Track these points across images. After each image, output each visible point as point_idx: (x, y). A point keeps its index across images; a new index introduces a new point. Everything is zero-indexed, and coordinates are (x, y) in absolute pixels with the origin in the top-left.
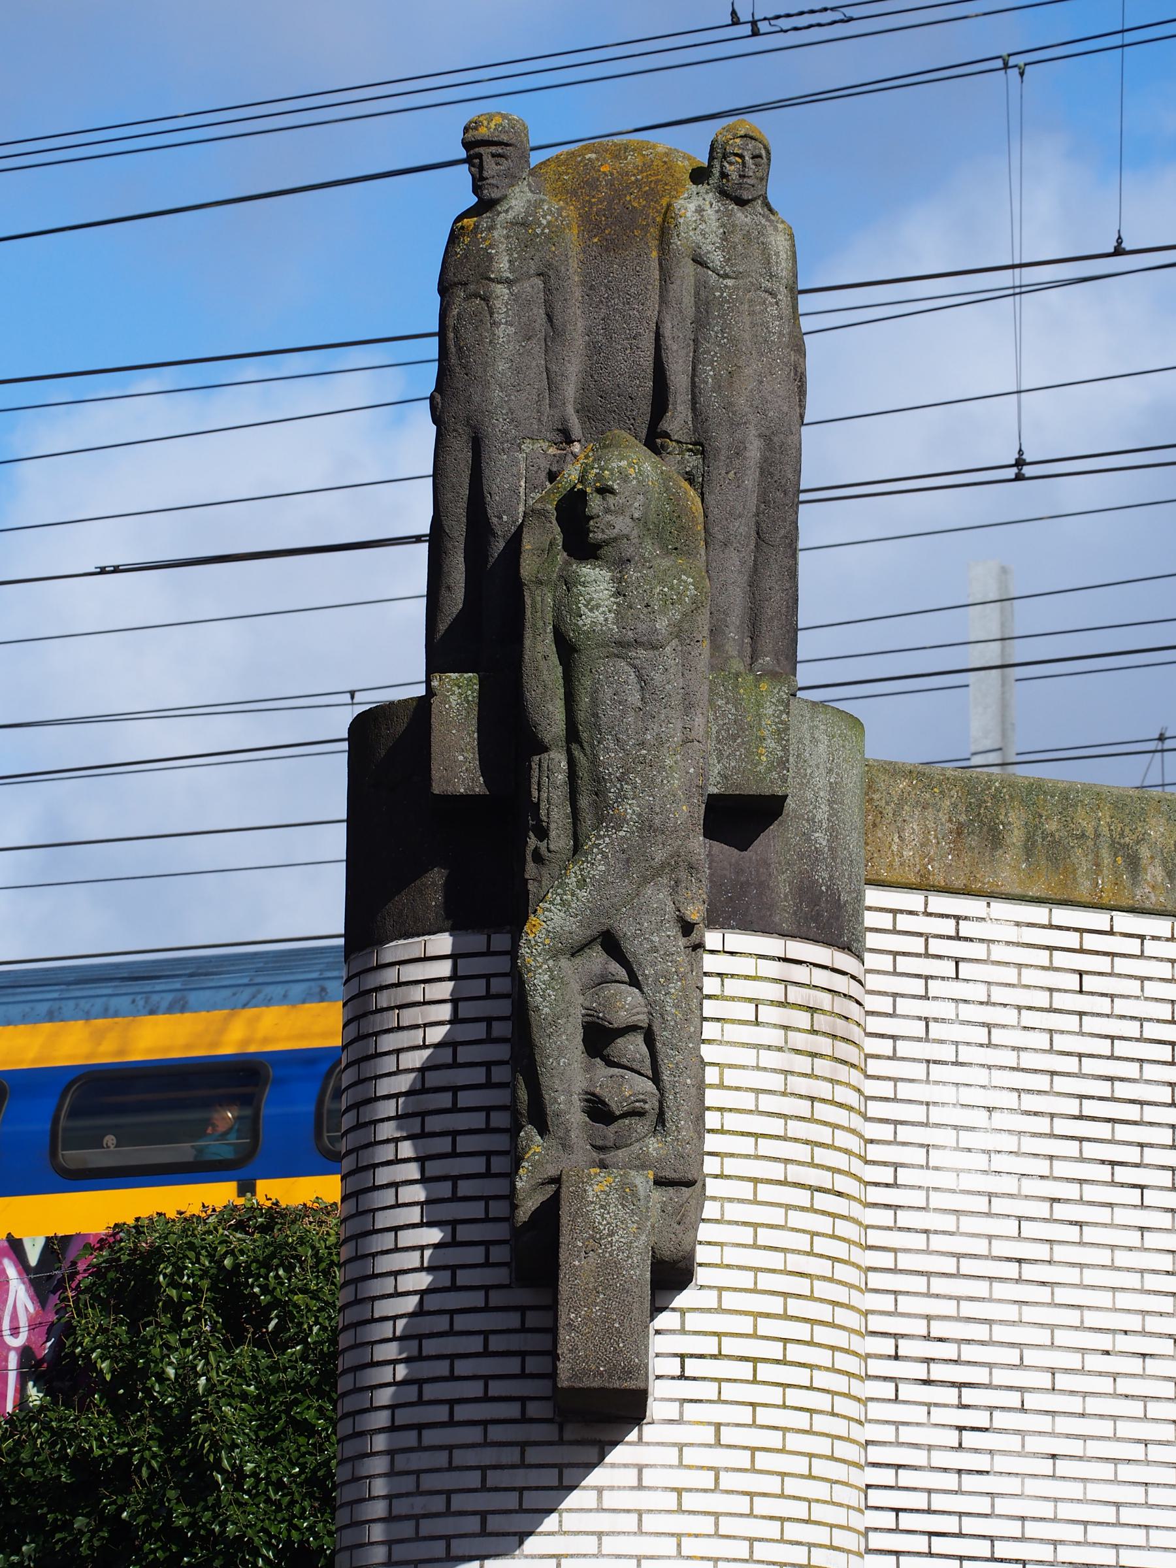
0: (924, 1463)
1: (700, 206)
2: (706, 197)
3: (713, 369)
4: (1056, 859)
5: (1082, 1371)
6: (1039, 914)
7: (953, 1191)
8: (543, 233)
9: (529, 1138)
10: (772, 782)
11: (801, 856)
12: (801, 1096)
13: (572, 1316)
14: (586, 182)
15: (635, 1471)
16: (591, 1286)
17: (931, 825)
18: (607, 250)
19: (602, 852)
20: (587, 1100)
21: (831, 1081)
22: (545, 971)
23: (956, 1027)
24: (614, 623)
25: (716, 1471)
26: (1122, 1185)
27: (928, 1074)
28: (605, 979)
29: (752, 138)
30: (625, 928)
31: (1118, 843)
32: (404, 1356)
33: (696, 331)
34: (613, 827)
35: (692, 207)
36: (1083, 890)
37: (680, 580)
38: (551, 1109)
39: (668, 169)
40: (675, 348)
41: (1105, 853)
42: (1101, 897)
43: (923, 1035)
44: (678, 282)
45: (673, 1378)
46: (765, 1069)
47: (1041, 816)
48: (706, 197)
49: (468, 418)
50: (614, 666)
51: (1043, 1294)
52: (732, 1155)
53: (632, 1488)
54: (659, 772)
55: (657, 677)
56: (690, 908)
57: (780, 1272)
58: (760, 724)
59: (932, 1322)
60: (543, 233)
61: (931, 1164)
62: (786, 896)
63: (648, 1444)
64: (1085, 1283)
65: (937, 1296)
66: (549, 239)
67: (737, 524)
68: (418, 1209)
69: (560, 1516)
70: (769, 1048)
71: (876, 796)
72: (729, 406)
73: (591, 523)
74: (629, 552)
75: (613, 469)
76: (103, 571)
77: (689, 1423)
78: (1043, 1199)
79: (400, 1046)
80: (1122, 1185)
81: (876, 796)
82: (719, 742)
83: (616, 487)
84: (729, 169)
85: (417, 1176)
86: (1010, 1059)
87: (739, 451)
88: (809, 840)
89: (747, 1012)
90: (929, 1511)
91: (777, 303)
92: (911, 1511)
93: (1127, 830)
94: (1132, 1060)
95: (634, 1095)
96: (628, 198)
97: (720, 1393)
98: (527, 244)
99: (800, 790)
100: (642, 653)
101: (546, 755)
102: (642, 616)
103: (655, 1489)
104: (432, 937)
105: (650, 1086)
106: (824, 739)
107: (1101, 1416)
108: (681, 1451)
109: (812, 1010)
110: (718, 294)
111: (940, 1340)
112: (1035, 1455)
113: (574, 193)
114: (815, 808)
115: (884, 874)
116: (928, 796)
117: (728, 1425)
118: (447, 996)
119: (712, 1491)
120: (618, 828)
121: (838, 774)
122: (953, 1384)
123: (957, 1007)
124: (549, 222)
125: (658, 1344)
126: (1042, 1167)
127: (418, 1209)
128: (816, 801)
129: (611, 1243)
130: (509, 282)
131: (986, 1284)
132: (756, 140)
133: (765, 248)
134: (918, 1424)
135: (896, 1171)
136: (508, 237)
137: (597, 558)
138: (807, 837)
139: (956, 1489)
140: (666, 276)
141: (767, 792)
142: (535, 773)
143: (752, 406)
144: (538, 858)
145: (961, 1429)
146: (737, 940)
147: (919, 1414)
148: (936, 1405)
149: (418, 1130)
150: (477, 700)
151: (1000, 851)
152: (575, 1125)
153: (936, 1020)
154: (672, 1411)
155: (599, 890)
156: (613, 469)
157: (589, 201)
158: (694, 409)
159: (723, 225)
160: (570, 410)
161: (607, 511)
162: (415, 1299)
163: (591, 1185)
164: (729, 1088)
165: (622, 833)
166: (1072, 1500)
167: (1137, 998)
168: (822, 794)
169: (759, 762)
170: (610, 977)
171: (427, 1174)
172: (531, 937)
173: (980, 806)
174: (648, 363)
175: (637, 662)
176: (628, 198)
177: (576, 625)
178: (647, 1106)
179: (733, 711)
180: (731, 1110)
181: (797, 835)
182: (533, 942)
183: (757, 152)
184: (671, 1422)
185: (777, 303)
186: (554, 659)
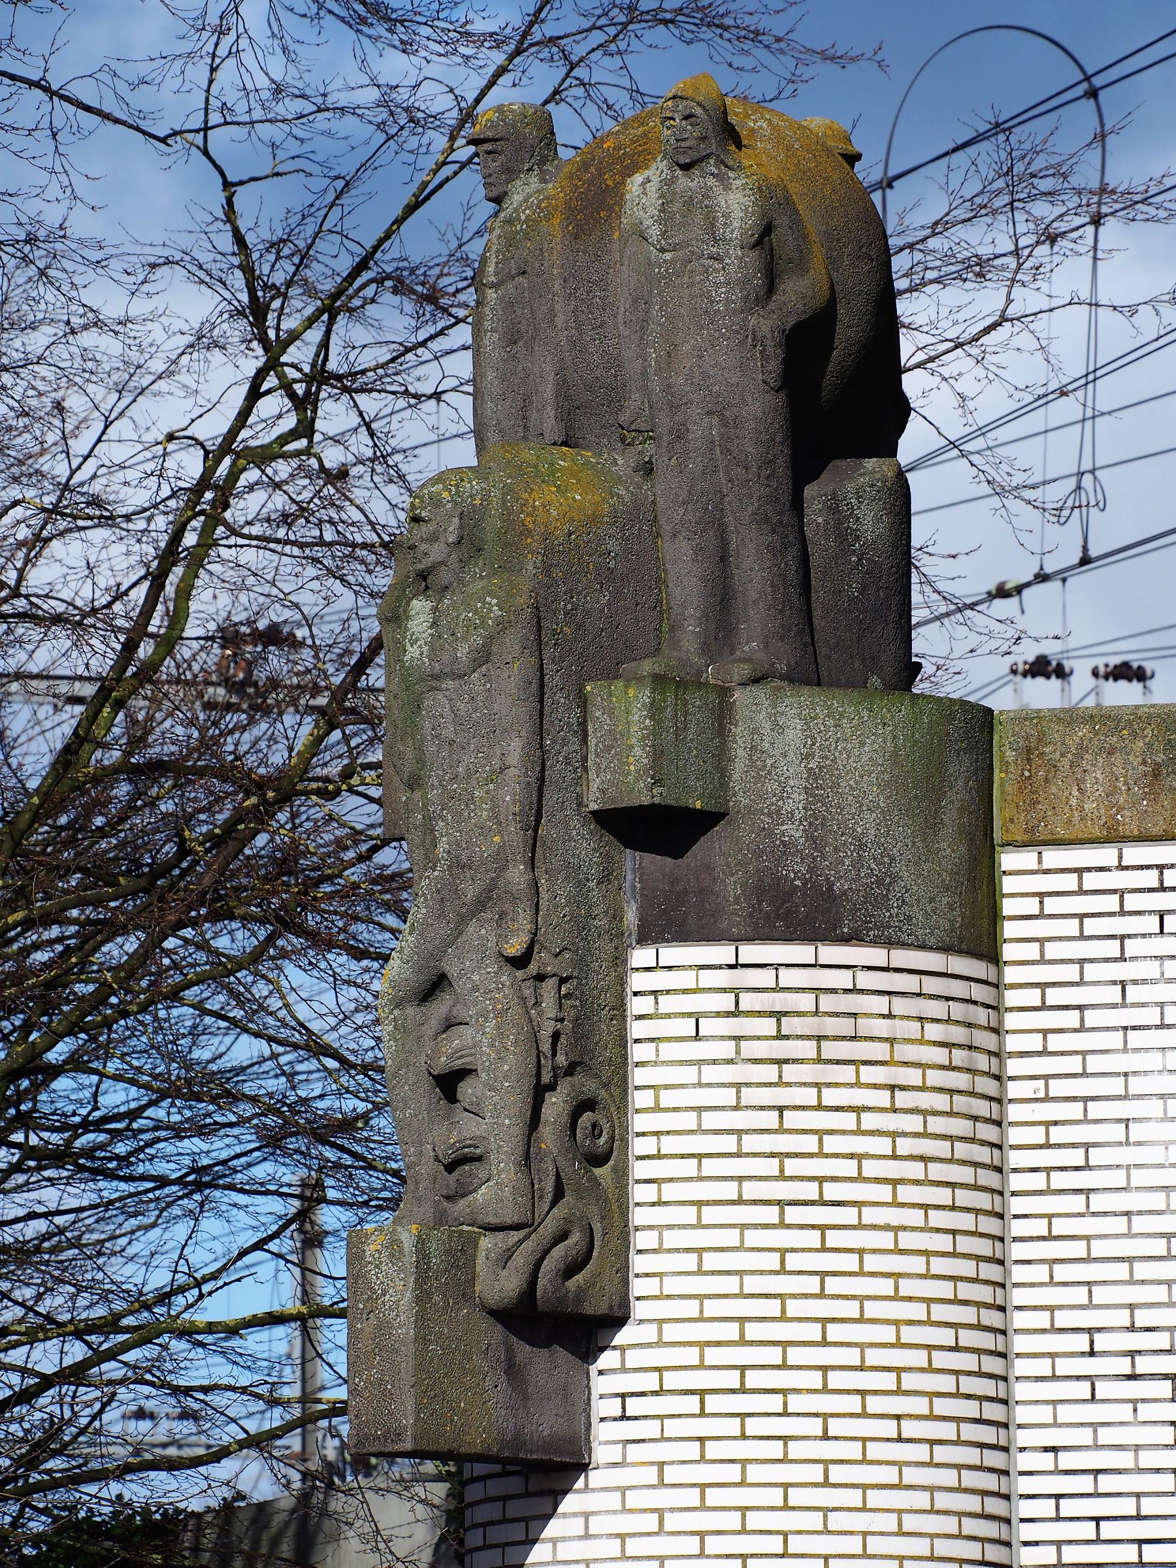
0: (1130, 1465)
11: (758, 854)
15: (582, 1520)
17: (1118, 771)
23: (1161, 987)
25: (660, 1512)
27: (1126, 1042)
37: (484, 603)
43: (1119, 1000)
46: (710, 1085)
52: (671, 1180)
57: (735, 1296)
59: (1137, 1312)
61: (1131, 1140)
62: (737, 898)
63: (593, 1490)
67: (681, 512)
70: (715, 1062)
71: (1047, 750)
77: (633, 1465)
81: (1047, 750)
88: (771, 834)
90: (1139, 1517)
92: (1115, 1518)
108: (623, 1495)
111: (1148, 1329)
114: (782, 798)
115: (1061, 832)
119: (656, 1534)
123: (1161, 965)
125: (600, 1385)
135: (1087, 1152)
146: (672, 954)
147: (1124, 1412)
153: (1135, 982)
154: (615, 1454)
168: (792, 783)
169: (629, 773)
178: (478, 1151)
184: (615, 1465)
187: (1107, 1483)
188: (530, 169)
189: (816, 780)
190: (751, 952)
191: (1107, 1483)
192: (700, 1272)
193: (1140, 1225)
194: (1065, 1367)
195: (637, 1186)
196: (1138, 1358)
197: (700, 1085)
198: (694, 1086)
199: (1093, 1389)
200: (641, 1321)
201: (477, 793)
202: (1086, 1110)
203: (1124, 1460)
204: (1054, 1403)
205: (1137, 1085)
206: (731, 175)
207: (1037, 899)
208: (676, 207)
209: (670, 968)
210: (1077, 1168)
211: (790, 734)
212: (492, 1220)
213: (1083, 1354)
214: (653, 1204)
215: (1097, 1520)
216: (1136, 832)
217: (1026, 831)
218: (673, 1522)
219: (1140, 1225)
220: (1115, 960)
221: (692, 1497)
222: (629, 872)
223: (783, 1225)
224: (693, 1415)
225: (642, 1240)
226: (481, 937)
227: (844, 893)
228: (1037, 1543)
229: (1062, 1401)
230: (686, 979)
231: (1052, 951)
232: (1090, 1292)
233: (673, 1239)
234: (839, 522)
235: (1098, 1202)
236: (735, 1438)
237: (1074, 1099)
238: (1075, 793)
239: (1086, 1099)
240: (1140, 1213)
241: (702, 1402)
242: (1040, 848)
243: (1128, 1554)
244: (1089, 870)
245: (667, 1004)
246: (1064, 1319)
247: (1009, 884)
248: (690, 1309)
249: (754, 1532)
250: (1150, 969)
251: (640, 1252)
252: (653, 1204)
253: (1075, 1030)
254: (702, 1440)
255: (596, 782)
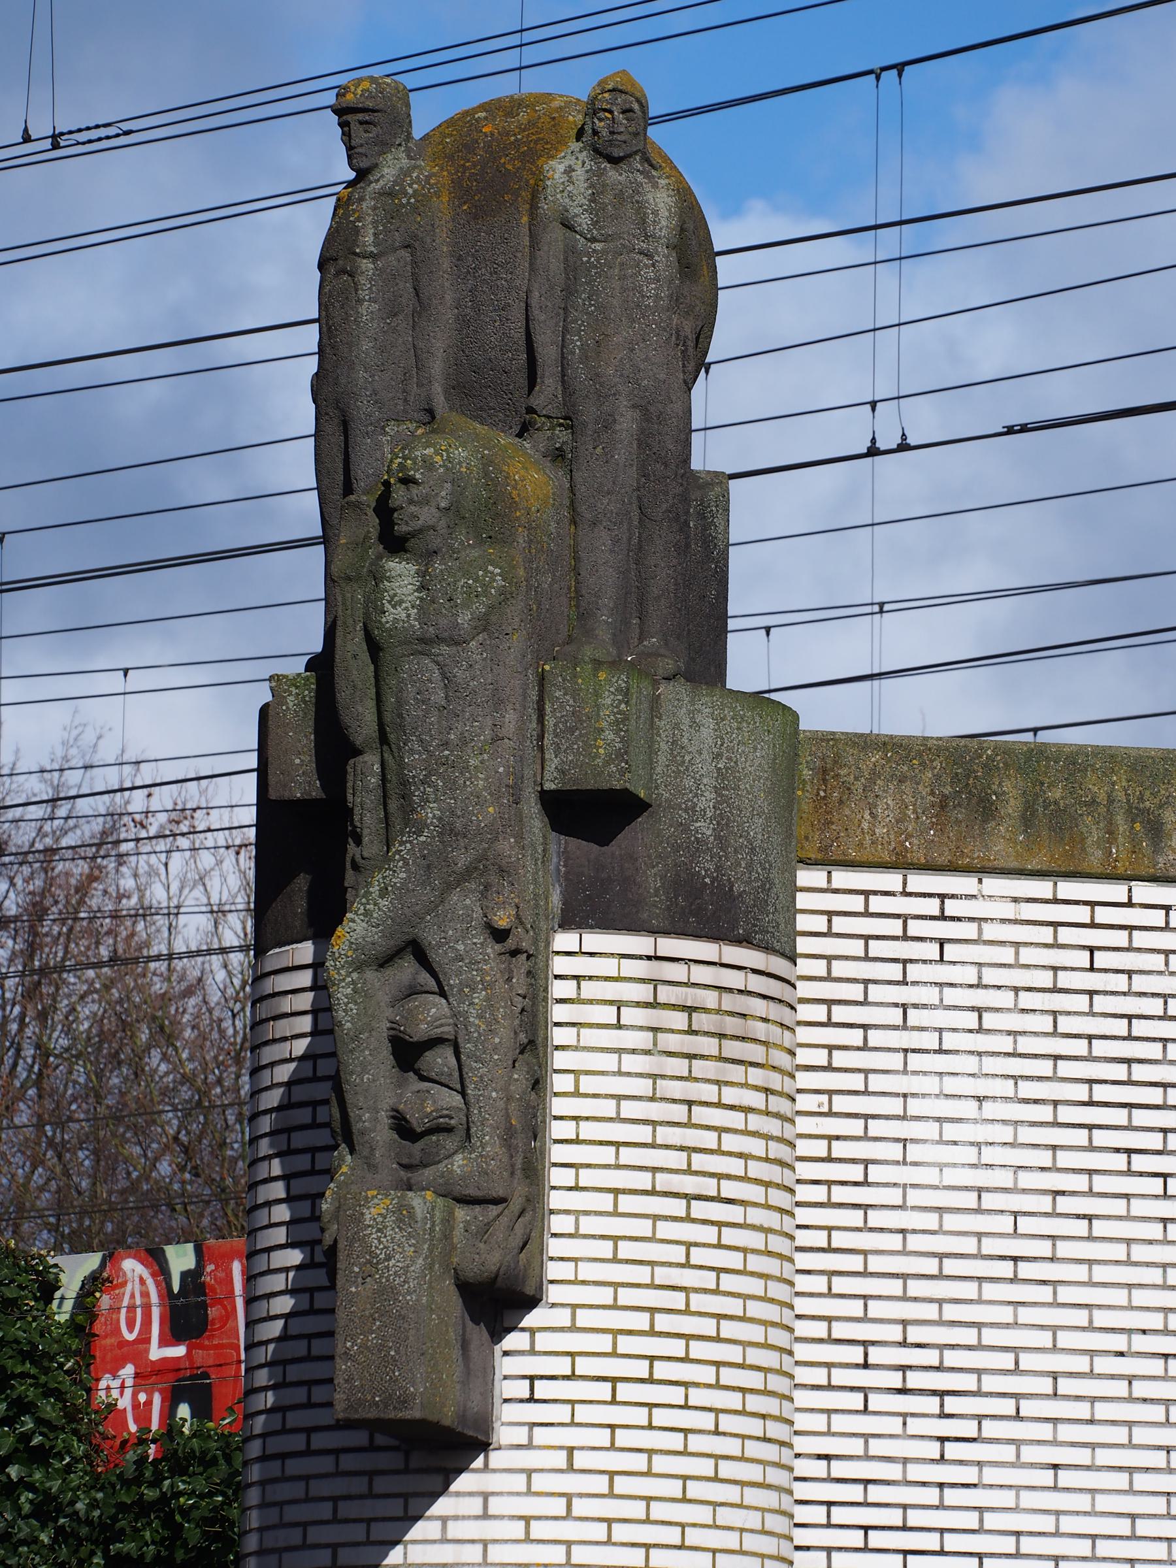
0: (898, 1476)
1: (570, 166)
2: (579, 155)
3: (580, 339)
4: (1060, 828)
5: (1091, 1375)
6: (1042, 888)
7: (936, 1187)
8: (408, 203)
9: (342, 1159)
10: (610, 776)
11: (676, 848)
12: (674, 1101)
13: (349, 1344)
14: (465, 146)
16: (367, 1313)
17: (909, 799)
18: (476, 217)
19: (403, 859)
20: (393, 1117)
21: (717, 1082)
22: (348, 984)
23: (940, 1013)
24: (415, 619)
25: (569, 1497)
26: (1141, 1174)
27: (906, 1063)
28: (413, 991)
29: (621, 91)
30: (430, 937)
31: (1137, 808)
32: (271, 1383)
33: (566, 299)
34: (414, 833)
35: (561, 168)
36: (1095, 859)
37: (486, 571)
38: (356, 1127)
39: (554, 126)
40: (542, 317)
41: (1120, 819)
42: (1115, 867)
43: (901, 1023)
44: (546, 248)
45: (521, 1401)
46: (629, 1074)
47: (1042, 784)
48: (579, 155)
49: (337, 401)
50: (418, 663)
51: (1045, 1294)
52: (589, 1166)
53: (477, 1518)
54: (461, 773)
55: (460, 674)
56: (501, 913)
57: (646, 1286)
58: (598, 715)
60: (408, 203)
61: (908, 1160)
62: (657, 890)
63: (494, 1471)
64: (1095, 1280)
65: (916, 1299)
66: (415, 209)
67: (605, 502)
68: (283, 1229)
69: (405, 1548)
70: (633, 1051)
71: (843, 772)
72: (596, 377)
73: (395, 515)
74: (435, 542)
75: (416, 458)
76: (1010, 431)
77: (540, 1447)
78: (1044, 1192)
79: (274, 1059)
80: (1141, 1174)
81: (843, 772)
82: (556, 736)
83: (418, 476)
84: (600, 125)
85: (283, 1195)
86: (1006, 1044)
87: (608, 424)
88: (687, 830)
89: (608, 1014)
90: (904, 1528)
91: (653, 265)
92: (883, 1528)
93: (1147, 793)
94: (1154, 1040)
95: (436, 1110)
96: (503, 161)
97: (573, 1415)
98: (393, 214)
99: (676, 778)
100: (445, 649)
101: (360, 758)
102: (444, 611)
103: (501, 1517)
104: (299, 945)
105: (459, 1097)
106: (711, 723)
107: (1114, 1423)
109: (690, 1010)
110: (585, 259)
112: (1033, 1465)
113: (451, 158)
114: (696, 795)
116: (906, 768)
117: (582, 1448)
118: (308, 1008)
120: (419, 833)
121: (730, 759)
122: (934, 1393)
123: (941, 992)
124: (415, 191)
125: (507, 1366)
126: (1045, 1158)
127: (283, 1229)
128: (698, 788)
129: (387, 1267)
130: (373, 256)
131: (975, 1285)
132: (626, 93)
133: (640, 208)
134: (891, 1436)
135: (866, 1168)
136: (375, 208)
137: (406, 551)
138: (685, 828)
139: (937, 1503)
140: (534, 244)
141: (606, 786)
142: (350, 778)
143: (622, 375)
144: (356, 867)
145: (943, 1440)
146: (595, 940)
147: (894, 1425)
148: (913, 1415)
149: (285, 1148)
150: (313, 700)
151: (993, 824)
152: (381, 1143)
153: (916, 1006)
154: (520, 1435)
155: (400, 898)
156: (416, 458)
157: (463, 165)
158: (563, 382)
159: (592, 186)
160: (438, 389)
161: (411, 502)
162: (280, 1323)
163: (369, 1208)
164: (586, 1095)
165: (422, 839)
166: (1077, 1513)
167: (1160, 973)
168: (705, 781)
169: (597, 755)
170: (419, 988)
171: (292, 1193)
172: (335, 949)
173: (968, 777)
174: (519, 335)
175: (440, 658)
176: (503, 161)
177: (380, 622)
178: (453, 1122)
179: (571, 702)
180: (587, 1119)
181: (671, 826)
182: (337, 955)
183: (628, 106)
184: (519, 1447)
185: (653, 265)
186: (365, 657)
187: (876, 1493)
188: (400, 145)
189: (723, 780)
190: (670, 946)
191: (876, 1493)
192: (615, 1260)
193: (915, 1243)
194: (840, 1377)
195: (553, 1169)
196: (909, 1374)
197: (620, 1073)
198: (614, 1074)
199: (866, 1400)
200: (553, 1305)
201: (472, 762)
202: (866, 1128)
203: (893, 1471)
204: (829, 1412)
205: (915, 1107)
206: (654, 173)
207: (825, 918)
208: (607, 198)
209: (592, 954)
210: (856, 1184)
211: (705, 732)
212: (472, 1192)
213: (857, 1366)
214: (570, 1189)
215: (866, 1529)
216: (923, 861)
217: (820, 850)
218: (581, 1507)
219: (915, 1243)
220: (897, 983)
221: (600, 1484)
222: (555, 855)
223: (688, 1219)
224: (605, 1403)
225: (558, 1224)
226: (466, 907)
227: (740, 895)
228: (808, 1548)
229: (836, 1411)
230: (608, 967)
231: (839, 969)
232: (866, 1305)
233: (589, 1225)
234: (705, 529)
235: (876, 1218)
236: (642, 1428)
237: (855, 1116)
238: (868, 817)
239: (867, 1117)
240: (914, 1231)
241: (614, 1390)
242: (830, 868)
243: (556, 1555)
244: (875, 893)
245: (589, 990)
246: (841, 1330)
247: (803, 900)
248: (604, 1295)
249: (657, 1522)
250: (930, 995)
251: (555, 1235)
252: (570, 1189)
253: (859, 1049)
254: (612, 1427)
255: (553, 763)
